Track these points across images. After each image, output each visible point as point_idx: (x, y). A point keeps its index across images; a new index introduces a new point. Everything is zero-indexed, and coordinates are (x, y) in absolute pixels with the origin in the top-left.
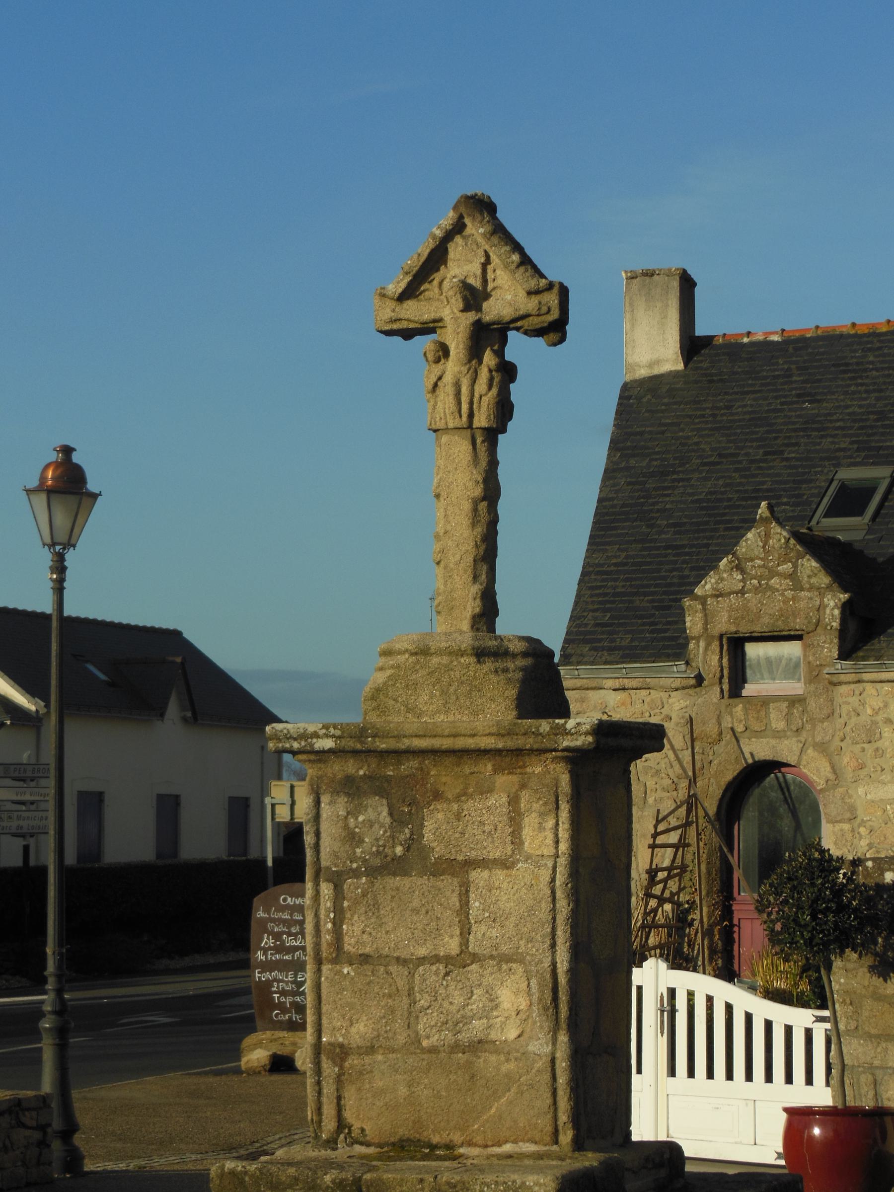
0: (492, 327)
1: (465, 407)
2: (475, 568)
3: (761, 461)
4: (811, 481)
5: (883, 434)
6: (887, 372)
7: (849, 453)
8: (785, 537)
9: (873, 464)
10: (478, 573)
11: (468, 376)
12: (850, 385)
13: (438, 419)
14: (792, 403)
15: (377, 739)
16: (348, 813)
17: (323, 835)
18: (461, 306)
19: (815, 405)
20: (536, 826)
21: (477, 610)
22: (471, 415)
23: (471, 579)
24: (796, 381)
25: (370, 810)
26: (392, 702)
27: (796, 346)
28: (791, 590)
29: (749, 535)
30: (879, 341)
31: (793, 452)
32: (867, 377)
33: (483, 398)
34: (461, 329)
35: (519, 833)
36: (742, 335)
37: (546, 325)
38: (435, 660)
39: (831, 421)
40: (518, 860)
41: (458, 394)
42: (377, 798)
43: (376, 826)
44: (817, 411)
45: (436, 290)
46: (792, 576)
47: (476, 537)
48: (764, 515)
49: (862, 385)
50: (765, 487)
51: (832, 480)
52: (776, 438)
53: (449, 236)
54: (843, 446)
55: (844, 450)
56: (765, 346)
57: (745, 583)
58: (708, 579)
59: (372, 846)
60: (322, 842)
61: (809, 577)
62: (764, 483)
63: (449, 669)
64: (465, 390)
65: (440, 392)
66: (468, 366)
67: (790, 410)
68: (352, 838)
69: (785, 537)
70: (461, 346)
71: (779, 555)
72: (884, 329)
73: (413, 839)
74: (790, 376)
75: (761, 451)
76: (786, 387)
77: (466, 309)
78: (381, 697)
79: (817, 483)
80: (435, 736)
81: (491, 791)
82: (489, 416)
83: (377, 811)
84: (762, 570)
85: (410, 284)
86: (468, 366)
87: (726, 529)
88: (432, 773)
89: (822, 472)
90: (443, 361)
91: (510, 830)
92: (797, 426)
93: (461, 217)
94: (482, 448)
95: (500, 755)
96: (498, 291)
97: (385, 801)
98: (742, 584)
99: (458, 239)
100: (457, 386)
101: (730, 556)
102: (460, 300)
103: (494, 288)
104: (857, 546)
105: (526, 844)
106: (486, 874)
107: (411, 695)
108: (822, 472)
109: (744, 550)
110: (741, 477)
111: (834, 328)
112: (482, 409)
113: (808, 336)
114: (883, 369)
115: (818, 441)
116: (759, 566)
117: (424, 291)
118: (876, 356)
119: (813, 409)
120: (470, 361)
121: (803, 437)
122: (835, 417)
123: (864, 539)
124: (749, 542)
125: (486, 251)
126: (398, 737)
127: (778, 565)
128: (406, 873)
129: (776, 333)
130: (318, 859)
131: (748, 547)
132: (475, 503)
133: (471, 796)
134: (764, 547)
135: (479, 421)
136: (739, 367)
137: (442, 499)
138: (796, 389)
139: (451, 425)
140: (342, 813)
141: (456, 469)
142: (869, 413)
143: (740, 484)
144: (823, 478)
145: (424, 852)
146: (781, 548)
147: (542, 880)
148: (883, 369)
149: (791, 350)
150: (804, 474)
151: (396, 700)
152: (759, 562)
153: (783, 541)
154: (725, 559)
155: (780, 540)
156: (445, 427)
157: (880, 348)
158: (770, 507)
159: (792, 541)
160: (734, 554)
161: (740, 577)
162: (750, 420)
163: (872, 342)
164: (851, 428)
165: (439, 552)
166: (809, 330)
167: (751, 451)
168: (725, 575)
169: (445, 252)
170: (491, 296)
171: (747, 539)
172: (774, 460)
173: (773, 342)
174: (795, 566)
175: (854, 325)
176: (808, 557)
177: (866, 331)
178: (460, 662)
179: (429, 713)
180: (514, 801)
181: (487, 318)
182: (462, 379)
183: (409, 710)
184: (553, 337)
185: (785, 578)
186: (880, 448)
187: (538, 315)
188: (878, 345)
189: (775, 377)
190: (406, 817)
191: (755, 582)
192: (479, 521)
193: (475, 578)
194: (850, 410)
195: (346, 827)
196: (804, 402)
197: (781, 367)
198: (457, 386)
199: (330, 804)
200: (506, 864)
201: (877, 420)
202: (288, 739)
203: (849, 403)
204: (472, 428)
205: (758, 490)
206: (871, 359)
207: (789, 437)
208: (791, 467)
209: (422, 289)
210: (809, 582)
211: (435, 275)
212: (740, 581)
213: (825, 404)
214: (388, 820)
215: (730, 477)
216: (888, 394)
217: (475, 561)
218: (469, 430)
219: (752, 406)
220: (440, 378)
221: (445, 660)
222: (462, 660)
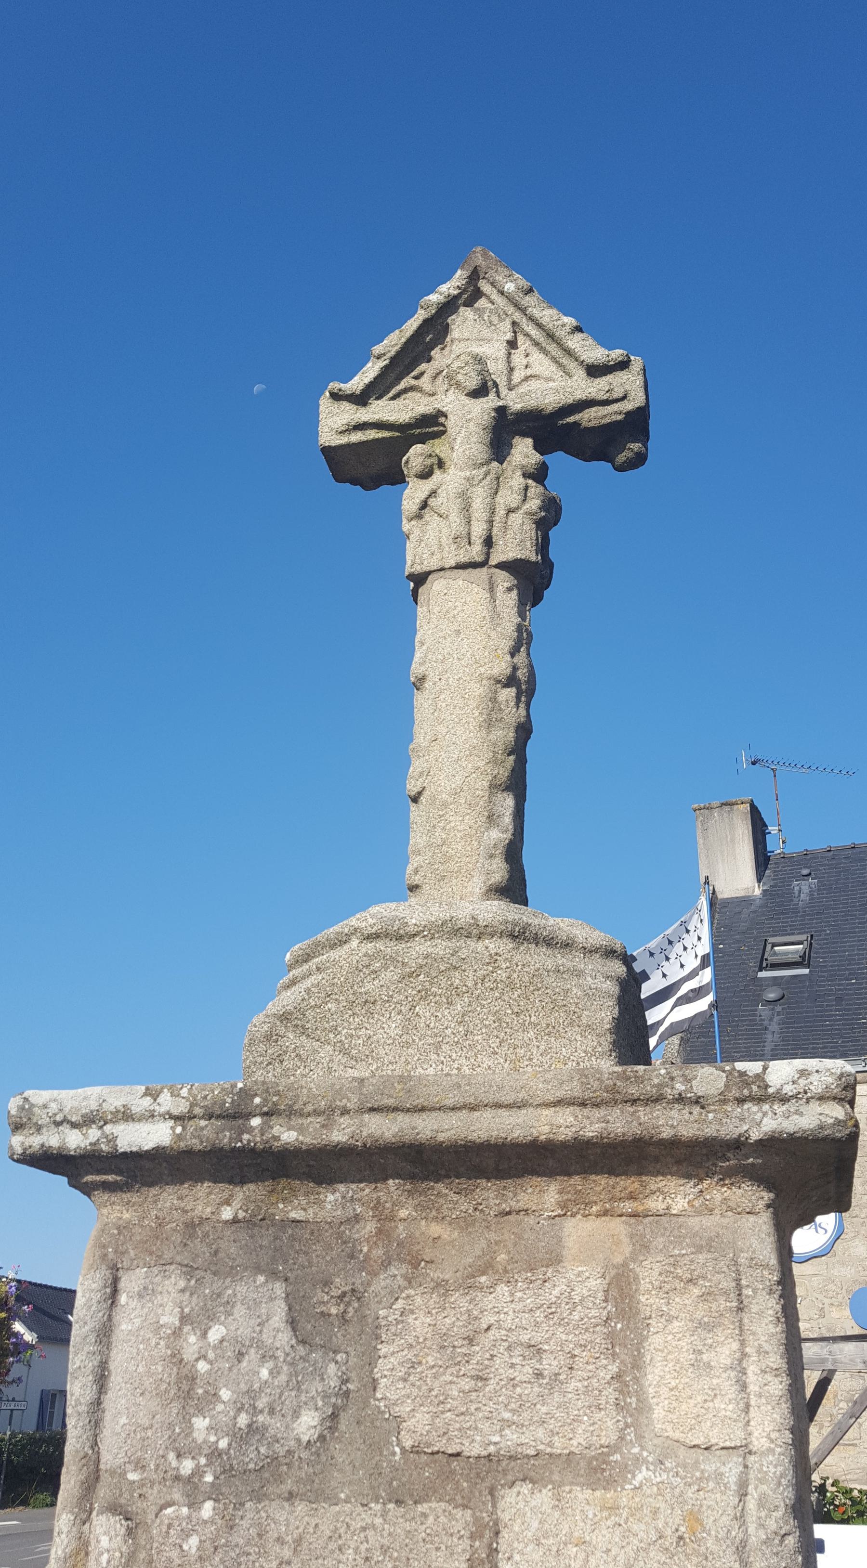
15: (274, 1120)
16: (184, 1319)
17: (116, 1380)
20: (687, 1357)
22: (489, 542)
25: (239, 1311)
35: (636, 1380)
37: (620, 417)
40: (638, 1461)
42: (261, 1279)
43: (253, 1355)
53: (449, 306)
59: (240, 1410)
60: (109, 1400)
64: (479, 504)
68: (187, 1391)
73: (347, 1393)
80: (423, 1109)
81: (555, 1260)
83: (259, 1311)
88: (403, 1213)
91: (614, 1368)
95: (766, 1069)
97: (279, 1288)
99: (465, 312)
105: (658, 1413)
106: (544, 1498)
126: (329, 1113)
128: (316, 1493)
130: (95, 1445)
133: (505, 1276)
140: (170, 1319)
145: (383, 1427)
147: (709, 1523)
180: (621, 1288)
190: (329, 1322)
193: (492, 819)
195: (176, 1359)
199: (140, 1296)
200: (599, 1469)
202: (58, 1124)
214: (285, 1338)
221: (441, 947)
222: (480, 946)
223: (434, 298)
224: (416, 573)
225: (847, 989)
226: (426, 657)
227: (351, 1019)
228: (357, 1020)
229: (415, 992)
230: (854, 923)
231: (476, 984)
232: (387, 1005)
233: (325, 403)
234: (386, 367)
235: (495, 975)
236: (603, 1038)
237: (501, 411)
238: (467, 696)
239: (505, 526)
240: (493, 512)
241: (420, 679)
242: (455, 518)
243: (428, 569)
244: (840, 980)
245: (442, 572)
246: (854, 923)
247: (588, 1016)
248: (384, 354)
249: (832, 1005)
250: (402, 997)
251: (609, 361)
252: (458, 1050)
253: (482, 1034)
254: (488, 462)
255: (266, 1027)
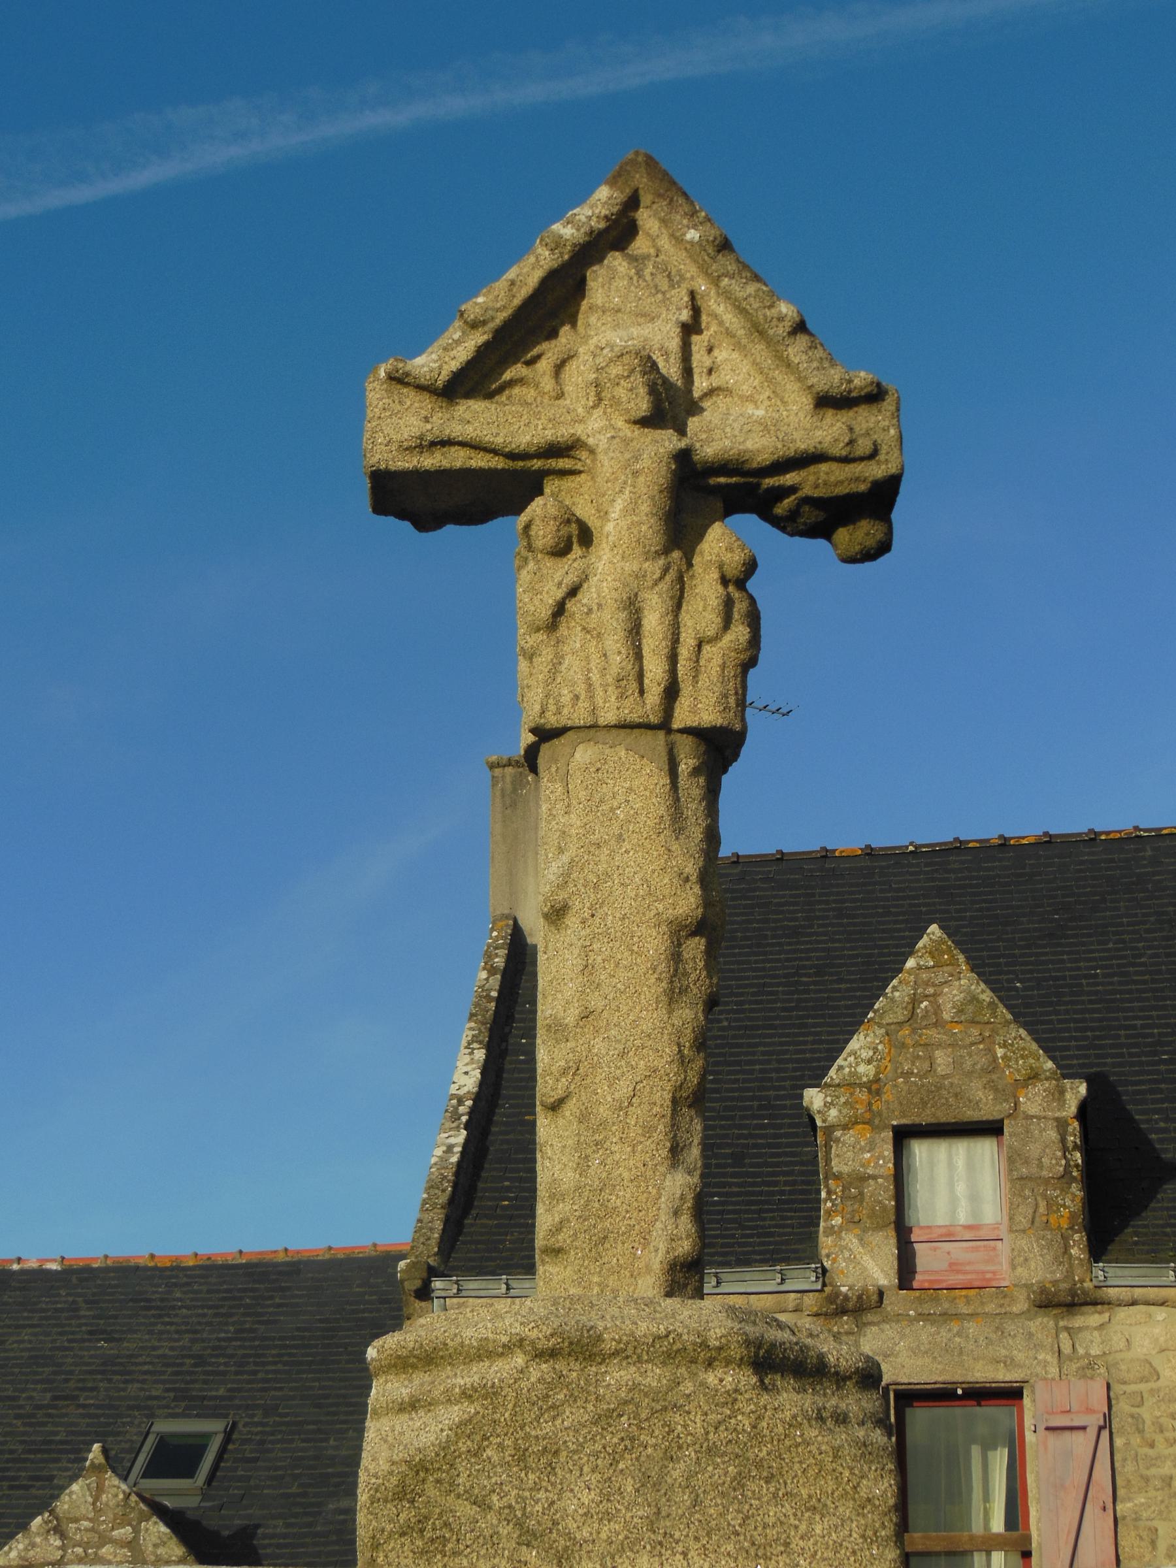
0: (713, 481)
1: (655, 669)
2: (674, 1125)
3: (48, 1406)
4: (118, 1434)
5: (205, 1382)
6: (200, 1311)
7: (164, 1402)
8: (124, 1492)
9: (198, 1416)
10: (683, 1136)
11: (664, 586)
12: (155, 1324)
13: (566, 698)
14: (83, 1341)
18: (643, 406)
19: (112, 1345)
21: (685, 1247)
22: (671, 692)
23: (664, 1153)
24: (85, 1316)
26: (466, 1510)
27: (78, 1277)
28: (130, 1563)
29: (75, 1487)
30: (186, 1276)
31: (92, 1398)
32: (176, 1315)
33: (707, 648)
34: (645, 462)
36: (11, 1261)
37: (863, 488)
38: (617, 1376)
39: (136, 1364)
41: (635, 631)
44: (116, 1352)
45: (548, 384)
46: (132, 1544)
47: (679, 1033)
48: (96, 1462)
49: (171, 1324)
50: (58, 1438)
51: (148, 1433)
52: (67, 1381)
54: (154, 1393)
55: (156, 1398)
56: (39, 1276)
57: (65, 1551)
58: (13, 1543)
61: (155, 1546)
62: (56, 1433)
63: (666, 1404)
64: (653, 621)
65: (572, 633)
66: (661, 562)
67: (81, 1349)
69: (124, 1492)
70: (645, 508)
71: (115, 1515)
72: (191, 1263)
74: (77, 1310)
75: (49, 1395)
76: (73, 1322)
77: (650, 421)
78: (432, 1491)
79: (128, 1437)
82: (726, 696)
84: (89, 1535)
85: (482, 352)
86: (661, 562)
87: (11, 1488)
89: (132, 1423)
90: (577, 551)
92: (93, 1368)
93: (632, 203)
94: (692, 789)
96: (720, 401)
98: (60, 1553)
99: (616, 261)
100: (633, 611)
101: (47, 1514)
102: (642, 391)
103: (711, 392)
104: (190, 1515)
107: (536, 1488)
108: (132, 1423)
109: (66, 1507)
110: (24, 1424)
111: (128, 1259)
112: (703, 677)
113: (95, 1265)
114: (195, 1307)
115: (122, 1386)
116: (86, 1530)
117: (511, 383)
118: (185, 1293)
119: (111, 1349)
120: (666, 551)
121: (101, 1381)
122: (140, 1360)
123: (199, 1508)
124: (74, 1497)
125: (692, 295)
127: (113, 1529)
129: (54, 1260)
131: (71, 1502)
132: (680, 932)
134: (94, 1504)
135: (694, 711)
136: (10, 1297)
137: (572, 921)
138: (86, 1325)
139: (609, 716)
141: (620, 838)
142: (183, 1357)
143: (24, 1434)
144: (134, 1430)
146: (118, 1506)
148: (195, 1307)
149: (74, 1280)
150: (108, 1424)
151: (483, 1504)
152: (86, 1524)
153: (121, 1496)
154: (39, 1518)
155: (116, 1495)
156: (589, 721)
157: (187, 1284)
158: (105, 1451)
159: (134, 1498)
160: (51, 1512)
161: (58, 1543)
162: (31, 1357)
163: (177, 1277)
164: (164, 1373)
165: (564, 1072)
166: (95, 1259)
167: (35, 1394)
168: (38, 1540)
169: (580, 289)
170: (702, 410)
171: (72, 1493)
172: (68, 1406)
173: (49, 1271)
174: (136, 1530)
175: (152, 1256)
176: (155, 1519)
177: (168, 1264)
178: (703, 1384)
179: (601, 1547)
181: (709, 450)
182: (644, 595)
183: (528, 1538)
184: (864, 532)
185: (122, 1547)
186: (204, 1398)
187: (846, 460)
188: (185, 1280)
189: (56, 1310)
191: (79, 1550)
192: (684, 991)
194: (160, 1352)
196: (99, 1340)
197: (63, 1299)
198: (633, 611)
201: (195, 1365)
203: (157, 1344)
204: (669, 731)
205: (51, 1442)
206: (178, 1295)
207: (83, 1380)
208: (90, 1416)
209: (507, 375)
210: (154, 1553)
211: (545, 346)
212: (59, 1548)
213: (125, 1344)
215: (10, 1425)
216: (205, 1336)
217: (675, 1101)
218: (661, 734)
219: (30, 1342)
220: (573, 592)
221: (655, 1376)
222: (711, 1378)
223: (566, 231)
224: (548, 726)
225: (751, 1136)
226: (569, 875)
227: (523, 1475)
228: (531, 1476)
229: (615, 1440)
230: (772, 1010)
231: (707, 1433)
232: (576, 1457)
233: (376, 393)
234: (487, 344)
235: (733, 1421)
236: (887, 1518)
237: (683, 457)
238: (635, 948)
239: (696, 671)
240: (675, 641)
241: (558, 911)
242: (615, 642)
243: (570, 723)
244: (743, 1117)
245: (593, 731)
246: (772, 1010)
247: (868, 1487)
248: (484, 323)
249: (725, 1166)
250: (598, 1447)
251: (850, 391)
252: (682, 1527)
253: (716, 1505)
254: (666, 551)
255: (394, 1480)
